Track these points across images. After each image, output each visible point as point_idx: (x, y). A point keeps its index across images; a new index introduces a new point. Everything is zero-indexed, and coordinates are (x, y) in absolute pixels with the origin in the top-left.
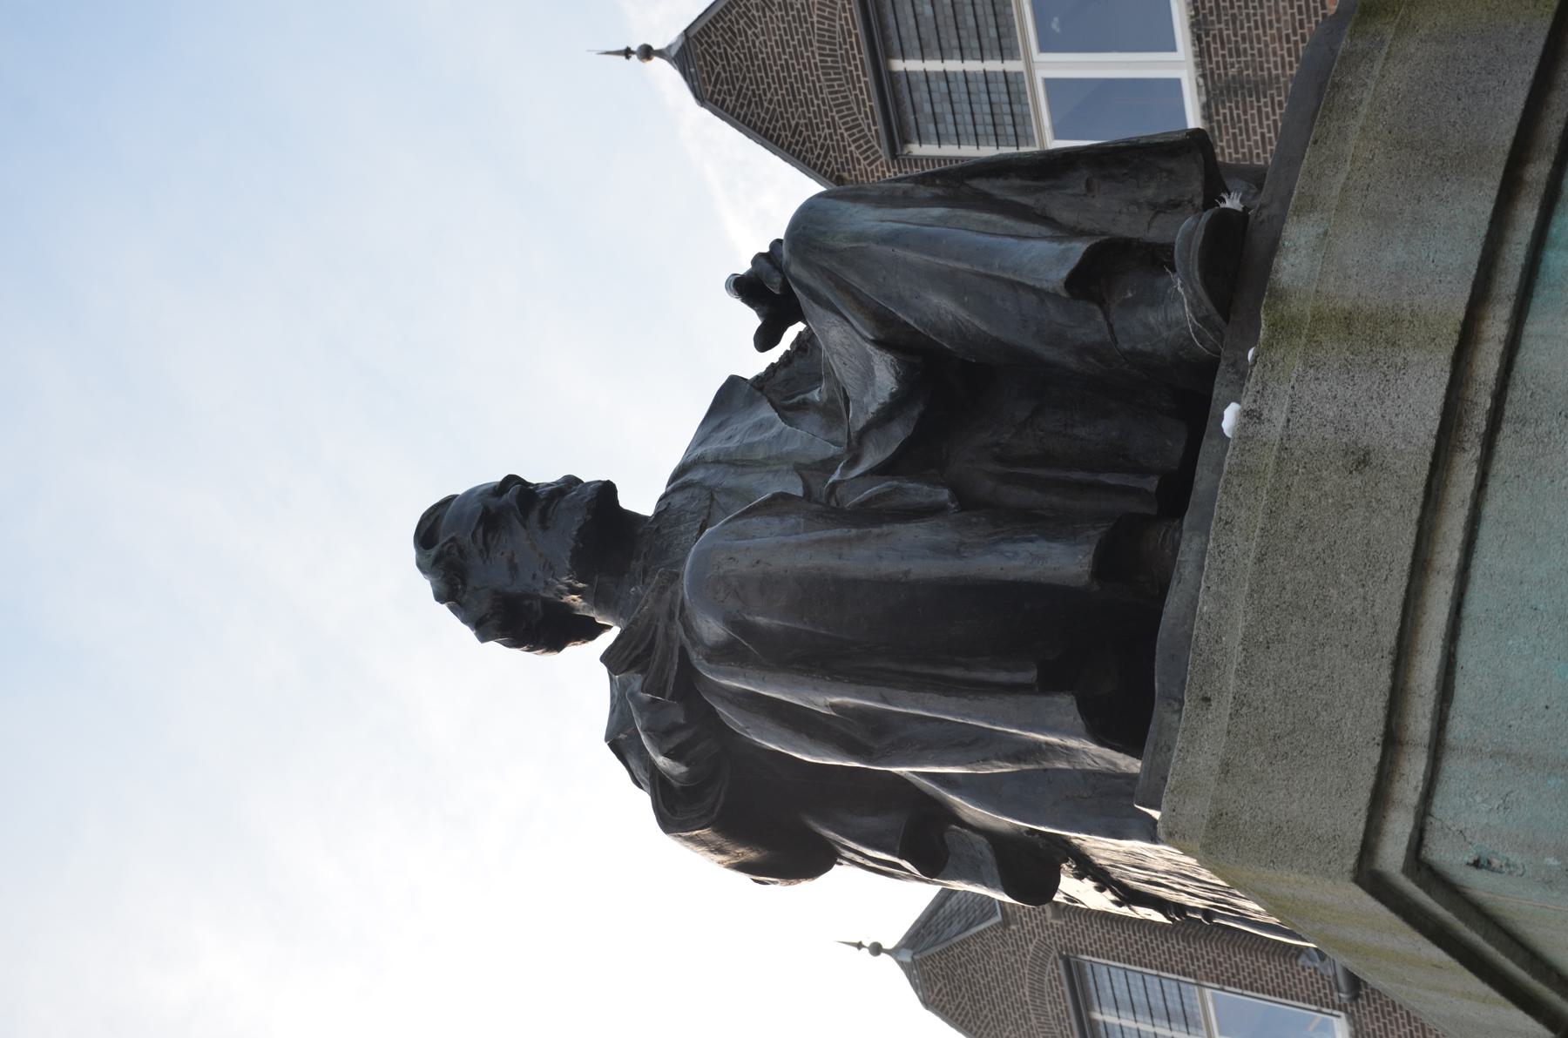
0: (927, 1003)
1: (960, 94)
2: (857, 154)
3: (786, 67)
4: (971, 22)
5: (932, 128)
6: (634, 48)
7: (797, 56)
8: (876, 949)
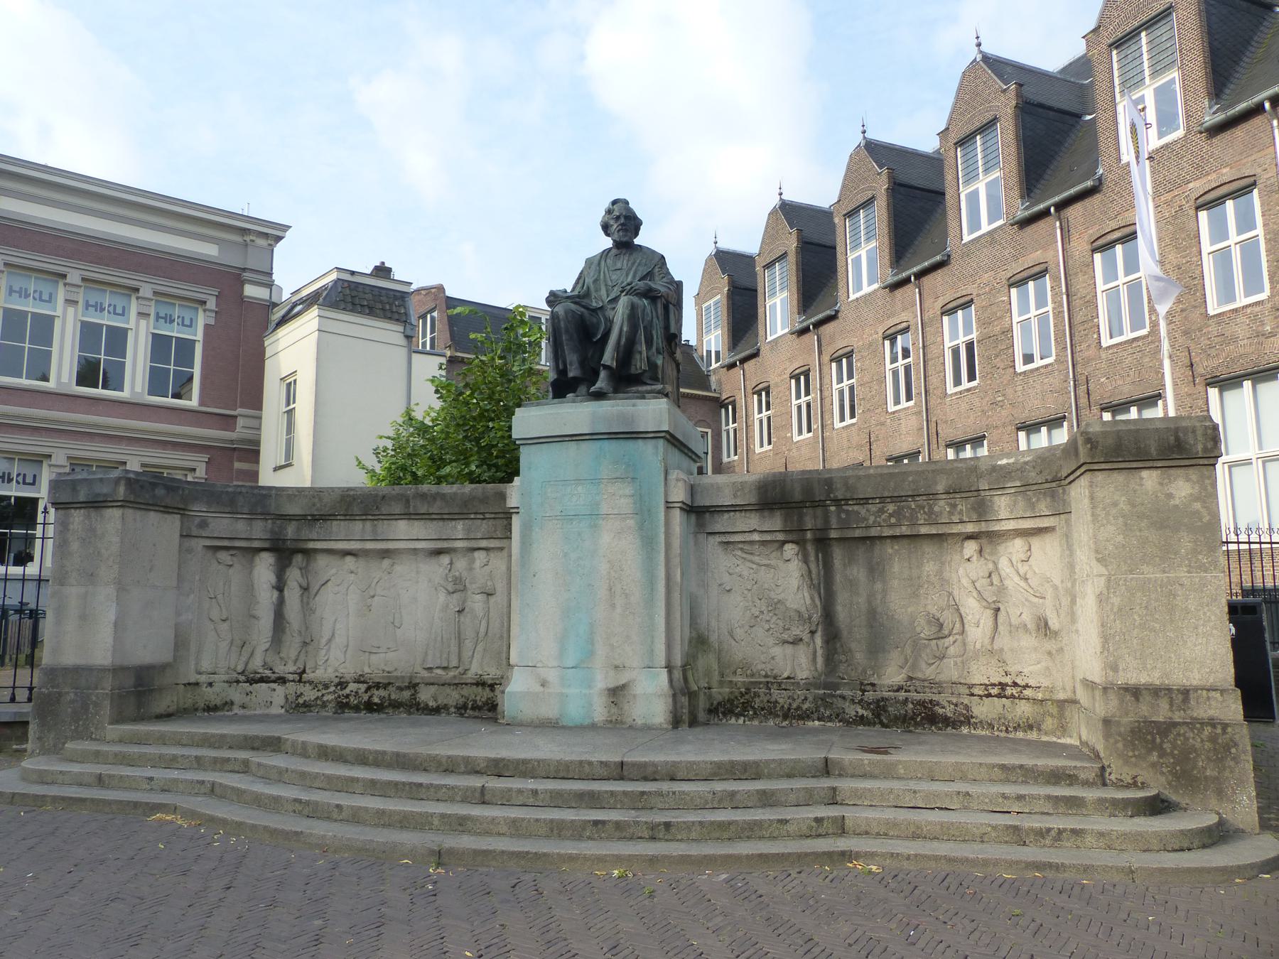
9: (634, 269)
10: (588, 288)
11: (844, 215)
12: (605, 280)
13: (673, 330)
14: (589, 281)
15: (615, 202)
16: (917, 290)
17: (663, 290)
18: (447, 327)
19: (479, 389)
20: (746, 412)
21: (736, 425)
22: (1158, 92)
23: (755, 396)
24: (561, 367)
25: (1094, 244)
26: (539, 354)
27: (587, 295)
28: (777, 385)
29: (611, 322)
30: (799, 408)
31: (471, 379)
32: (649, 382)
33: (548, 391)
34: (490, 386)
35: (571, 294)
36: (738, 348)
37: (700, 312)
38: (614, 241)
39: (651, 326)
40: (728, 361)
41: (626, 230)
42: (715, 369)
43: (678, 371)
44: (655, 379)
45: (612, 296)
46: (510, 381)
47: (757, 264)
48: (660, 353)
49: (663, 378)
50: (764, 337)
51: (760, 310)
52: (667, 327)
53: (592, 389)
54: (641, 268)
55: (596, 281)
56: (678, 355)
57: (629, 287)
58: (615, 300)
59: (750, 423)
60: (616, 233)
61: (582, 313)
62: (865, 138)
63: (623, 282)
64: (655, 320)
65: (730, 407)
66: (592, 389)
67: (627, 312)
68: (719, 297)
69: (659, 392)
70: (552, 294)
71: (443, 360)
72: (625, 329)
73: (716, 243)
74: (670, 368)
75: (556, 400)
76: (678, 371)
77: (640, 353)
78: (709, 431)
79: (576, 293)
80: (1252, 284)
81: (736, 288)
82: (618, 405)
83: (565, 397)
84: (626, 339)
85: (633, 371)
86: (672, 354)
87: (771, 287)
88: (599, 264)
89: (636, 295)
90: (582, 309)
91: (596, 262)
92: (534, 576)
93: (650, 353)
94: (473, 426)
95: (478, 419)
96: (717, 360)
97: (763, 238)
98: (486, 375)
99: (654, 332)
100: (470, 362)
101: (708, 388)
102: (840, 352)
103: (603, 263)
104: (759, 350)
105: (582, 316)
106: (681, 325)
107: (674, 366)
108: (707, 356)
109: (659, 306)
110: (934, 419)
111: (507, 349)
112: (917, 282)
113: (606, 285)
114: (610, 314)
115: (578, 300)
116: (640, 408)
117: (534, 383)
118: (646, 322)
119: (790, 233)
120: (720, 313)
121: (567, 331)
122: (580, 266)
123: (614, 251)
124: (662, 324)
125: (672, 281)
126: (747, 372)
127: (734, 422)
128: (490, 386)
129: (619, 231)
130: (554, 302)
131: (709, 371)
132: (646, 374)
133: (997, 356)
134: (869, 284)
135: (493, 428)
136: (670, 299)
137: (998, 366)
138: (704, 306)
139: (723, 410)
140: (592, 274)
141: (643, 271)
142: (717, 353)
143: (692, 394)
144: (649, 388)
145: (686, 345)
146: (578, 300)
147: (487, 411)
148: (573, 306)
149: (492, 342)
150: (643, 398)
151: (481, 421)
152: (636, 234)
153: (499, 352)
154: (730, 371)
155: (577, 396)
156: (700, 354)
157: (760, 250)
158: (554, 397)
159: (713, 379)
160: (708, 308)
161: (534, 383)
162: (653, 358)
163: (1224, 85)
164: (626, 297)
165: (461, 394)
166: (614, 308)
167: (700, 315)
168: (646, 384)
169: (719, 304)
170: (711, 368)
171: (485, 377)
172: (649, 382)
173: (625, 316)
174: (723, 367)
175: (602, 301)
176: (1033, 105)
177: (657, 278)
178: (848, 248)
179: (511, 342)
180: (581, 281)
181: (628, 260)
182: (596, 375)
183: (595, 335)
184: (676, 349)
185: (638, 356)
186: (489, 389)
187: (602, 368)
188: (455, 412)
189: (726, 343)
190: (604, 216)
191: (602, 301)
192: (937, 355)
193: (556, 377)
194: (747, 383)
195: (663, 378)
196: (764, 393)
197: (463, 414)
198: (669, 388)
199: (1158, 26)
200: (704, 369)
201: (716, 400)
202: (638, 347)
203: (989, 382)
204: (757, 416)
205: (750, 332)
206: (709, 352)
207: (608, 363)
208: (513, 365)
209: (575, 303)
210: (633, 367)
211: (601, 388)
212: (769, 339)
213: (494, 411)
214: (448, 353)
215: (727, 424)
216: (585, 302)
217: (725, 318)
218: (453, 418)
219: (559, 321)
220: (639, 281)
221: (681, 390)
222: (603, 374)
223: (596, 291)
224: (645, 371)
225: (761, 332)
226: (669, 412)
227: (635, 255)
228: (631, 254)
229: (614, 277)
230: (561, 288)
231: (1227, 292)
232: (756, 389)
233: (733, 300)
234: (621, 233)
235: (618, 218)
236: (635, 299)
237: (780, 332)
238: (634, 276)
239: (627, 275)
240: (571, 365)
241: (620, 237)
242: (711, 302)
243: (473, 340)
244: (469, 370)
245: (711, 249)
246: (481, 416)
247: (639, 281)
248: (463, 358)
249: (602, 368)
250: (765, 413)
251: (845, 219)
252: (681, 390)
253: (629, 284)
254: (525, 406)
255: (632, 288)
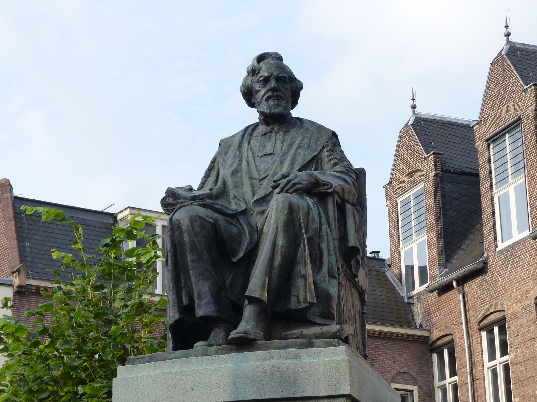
9: (291, 153)
10: (224, 183)
11: (487, 140)
12: (249, 172)
13: (352, 241)
14: (225, 172)
15: (261, 58)
16: (461, 296)
17: (336, 183)
18: (15, 242)
19: (64, 335)
20: (471, 357)
21: (455, 378)
23: (484, 334)
24: (185, 302)
25: (481, 324)
26: (153, 282)
27: (223, 193)
28: (516, 316)
29: (260, 232)
30: (494, 372)
31: (50, 322)
32: (318, 320)
33: (165, 337)
34: (80, 330)
35: (198, 193)
36: (454, 261)
37: (394, 209)
38: (262, 113)
39: (320, 237)
40: (440, 281)
41: (279, 98)
42: (421, 294)
43: (363, 302)
44: (328, 316)
45: (260, 194)
46: (109, 323)
47: (477, 136)
48: (335, 277)
49: (339, 314)
50: (492, 244)
51: (485, 205)
52: (343, 238)
53: (233, 334)
54: (302, 152)
55: (235, 173)
56: (362, 278)
57: (284, 181)
58: (265, 200)
59: (477, 375)
60: (264, 102)
61: (216, 220)
62: (508, 42)
63: (275, 173)
64: (325, 227)
65: (446, 351)
66: (233, 334)
67: (283, 217)
68: (421, 186)
69: (334, 336)
70: (171, 193)
71: (8, 293)
72: (280, 242)
73: (414, 107)
74: (350, 299)
75: (178, 353)
76: (363, 302)
77: (304, 277)
78: (415, 389)
79: (206, 190)
81: (447, 172)
82: (272, 358)
83: (191, 347)
84: (282, 258)
85: (293, 305)
86: (352, 277)
87: (500, 170)
88: (240, 147)
89: (296, 191)
90: (216, 215)
91: (235, 144)
93: (318, 278)
94: (55, 393)
95: (62, 382)
96: (423, 280)
97: (485, 99)
98: (72, 314)
99: (324, 246)
100: (49, 293)
101: (410, 323)
102: (492, 318)
103: (245, 145)
104: (485, 263)
105: (215, 226)
106: (364, 235)
107: (356, 295)
108: (407, 274)
109: (331, 207)
111: (106, 276)
112: (460, 287)
113: (251, 178)
114: (257, 220)
115: (209, 201)
116: (306, 361)
117: (146, 325)
118: (311, 232)
119: (525, 91)
120: (423, 210)
121: (193, 249)
122: (213, 150)
123: (262, 128)
124: (336, 233)
125: (349, 169)
126: (469, 297)
127: (453, 373)
128: (80, 330)
129: (267, 99)
130: (173, 205)
131: (411, 297)
132: (314, 310)
134: (519, 232)
135: (84, 394)
136: (346, 197)
138: (399, 200)
139: (435, 357)
140: (229, 162)
141: (305, 155)
142: (423, 270)
143: (392, 333)
144: (317, 330)
145: (374, 258)
146: (209, 201)
147: (74, 368)
148: (202, 212)
149: (83, 265)
150: (310, 345)
151: (65, 384)
152: (294, 103)
153: (93, 280)
154: (444, 297)
155: (210, 345)
156: (396, 271)
157: (482, 112)
158: (176, 348)
159: (417, 308)
160: (407, 203)
161: (146, 325)
162: (323, 285)
163: (455, 251)
164: (280, 196)
165: (36, 344)
166: (263, 212)
167: (393, 213)
168: (314, 324)
169: (423, 197)
170: (414, 293)
171: (71, 318)
172: (318, 320)
173: (281, 224)
174: (432, 291)
175: (246, 202)
176: (454, 173)
177: (326, 166)
178: (494, 182)
179: (110, 265)
180: (214, 173)
181: (283, 141)
182: (239, 311)
183: (236, 253)
184: (358, 269)
185: (300, 283)
186: (78, 335)
187: (246, 302)
188: (26, 371)
189: (436, 254)
190: (246, 79)
191: (246, 202)
193: (177, 316)
194: (470, 313)
195: (339, 314)
196: (496, 329)
197: (38, 374)
198: (349, 330)
199: (500, 142)
200: (403, 294)
201: (424, 340)
202: (300, 269)
204: (487, 364)
205: (471, 237)
206: (410, 269)
207: (256, 294)
208: (114, 300)
209: (205, 206)
210: (293, 299)
211: (245, 333)
212: (501, 246)
213: (85, 369)
214: (17, 281)
215: (442, 377)
216: (220, 203)
217: (432, 217)
218: (23, 379)
219: (181, 234)
220: (300, 170)
221: (368, 327)
222: (248, 311)
223: (236, 187)
224: (311, 305)
225: (488, 237)
226: (351, 367)
227: (292, 133)
228: (287, 132)
229: (262, 166)
230: (184, 184)
232: (485, 322)
233: (443, 189)
234: (271, 103)
235: (266, 80)
236: (295, 198)
237: (517, 237)
238: (292, 164)
239: (282, 163)
240: (200, 298)
241: (269, 107)
242: (411, 194)
243: (57, 260)
244: (48, 308)
245: (408, 117)
246: (67, 376)
247: (300, 170)
248: (38, 288)
249: (246, 302)
250: (499, 360)
251: (489, 145)
252: (368, 327)
253: (284, 177)
254: (133, 362)
255: (289, 182)
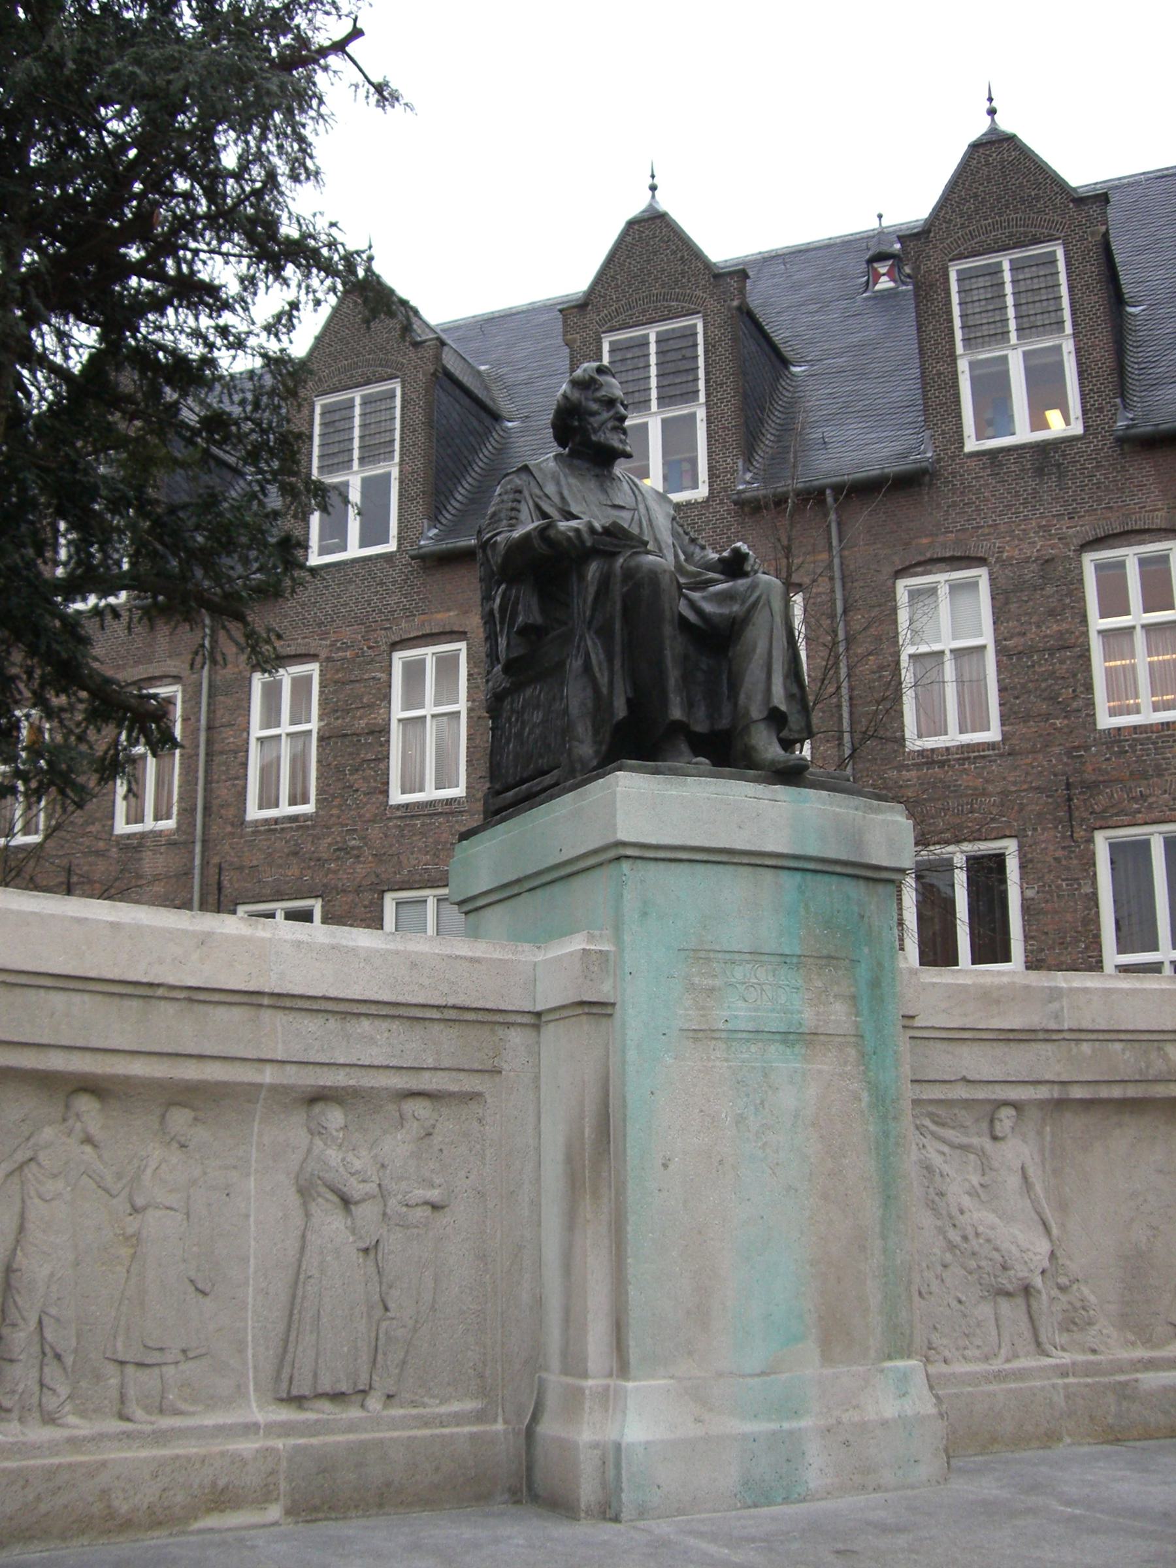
0: (631, 224)
1: (671, 367)
2: (602, 314)
3: (650, 273)
4: (678, 380)
5: (619, 358)
6: (994, 104)
7: (656, 279)
8: (992, 112)
22: (365, 482)
80: (973, 719)
92: (665, 1166)
110: (215, 860)
133: (355, 770)
137: (356, 786)
192: (232, 747)
203: (335, 811)
231: (269, 799)
